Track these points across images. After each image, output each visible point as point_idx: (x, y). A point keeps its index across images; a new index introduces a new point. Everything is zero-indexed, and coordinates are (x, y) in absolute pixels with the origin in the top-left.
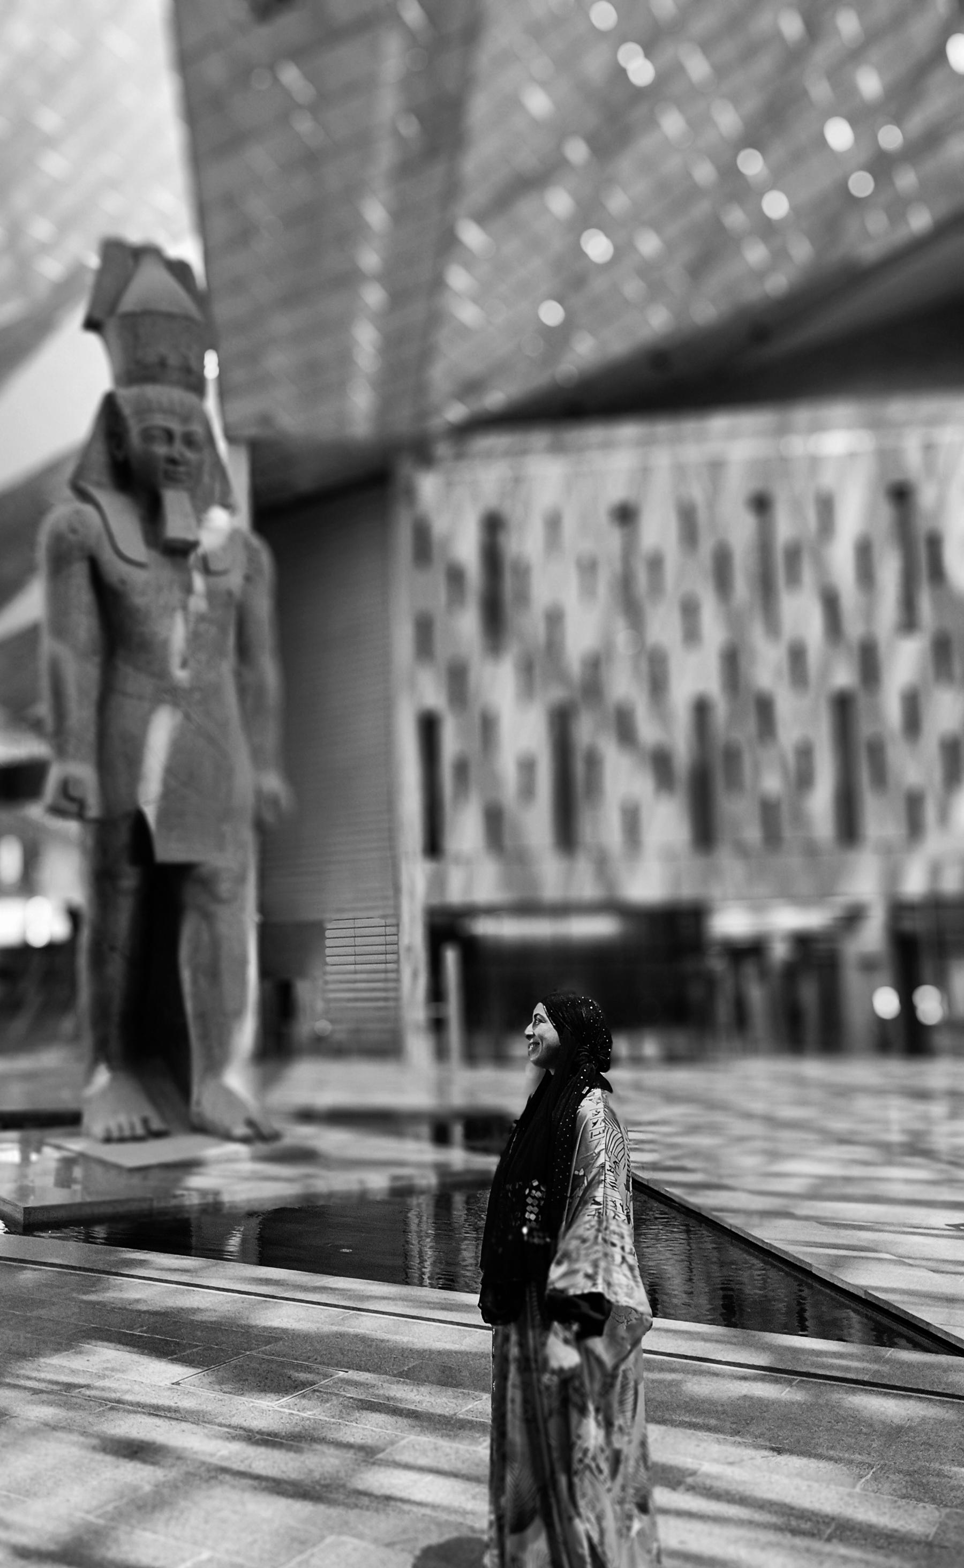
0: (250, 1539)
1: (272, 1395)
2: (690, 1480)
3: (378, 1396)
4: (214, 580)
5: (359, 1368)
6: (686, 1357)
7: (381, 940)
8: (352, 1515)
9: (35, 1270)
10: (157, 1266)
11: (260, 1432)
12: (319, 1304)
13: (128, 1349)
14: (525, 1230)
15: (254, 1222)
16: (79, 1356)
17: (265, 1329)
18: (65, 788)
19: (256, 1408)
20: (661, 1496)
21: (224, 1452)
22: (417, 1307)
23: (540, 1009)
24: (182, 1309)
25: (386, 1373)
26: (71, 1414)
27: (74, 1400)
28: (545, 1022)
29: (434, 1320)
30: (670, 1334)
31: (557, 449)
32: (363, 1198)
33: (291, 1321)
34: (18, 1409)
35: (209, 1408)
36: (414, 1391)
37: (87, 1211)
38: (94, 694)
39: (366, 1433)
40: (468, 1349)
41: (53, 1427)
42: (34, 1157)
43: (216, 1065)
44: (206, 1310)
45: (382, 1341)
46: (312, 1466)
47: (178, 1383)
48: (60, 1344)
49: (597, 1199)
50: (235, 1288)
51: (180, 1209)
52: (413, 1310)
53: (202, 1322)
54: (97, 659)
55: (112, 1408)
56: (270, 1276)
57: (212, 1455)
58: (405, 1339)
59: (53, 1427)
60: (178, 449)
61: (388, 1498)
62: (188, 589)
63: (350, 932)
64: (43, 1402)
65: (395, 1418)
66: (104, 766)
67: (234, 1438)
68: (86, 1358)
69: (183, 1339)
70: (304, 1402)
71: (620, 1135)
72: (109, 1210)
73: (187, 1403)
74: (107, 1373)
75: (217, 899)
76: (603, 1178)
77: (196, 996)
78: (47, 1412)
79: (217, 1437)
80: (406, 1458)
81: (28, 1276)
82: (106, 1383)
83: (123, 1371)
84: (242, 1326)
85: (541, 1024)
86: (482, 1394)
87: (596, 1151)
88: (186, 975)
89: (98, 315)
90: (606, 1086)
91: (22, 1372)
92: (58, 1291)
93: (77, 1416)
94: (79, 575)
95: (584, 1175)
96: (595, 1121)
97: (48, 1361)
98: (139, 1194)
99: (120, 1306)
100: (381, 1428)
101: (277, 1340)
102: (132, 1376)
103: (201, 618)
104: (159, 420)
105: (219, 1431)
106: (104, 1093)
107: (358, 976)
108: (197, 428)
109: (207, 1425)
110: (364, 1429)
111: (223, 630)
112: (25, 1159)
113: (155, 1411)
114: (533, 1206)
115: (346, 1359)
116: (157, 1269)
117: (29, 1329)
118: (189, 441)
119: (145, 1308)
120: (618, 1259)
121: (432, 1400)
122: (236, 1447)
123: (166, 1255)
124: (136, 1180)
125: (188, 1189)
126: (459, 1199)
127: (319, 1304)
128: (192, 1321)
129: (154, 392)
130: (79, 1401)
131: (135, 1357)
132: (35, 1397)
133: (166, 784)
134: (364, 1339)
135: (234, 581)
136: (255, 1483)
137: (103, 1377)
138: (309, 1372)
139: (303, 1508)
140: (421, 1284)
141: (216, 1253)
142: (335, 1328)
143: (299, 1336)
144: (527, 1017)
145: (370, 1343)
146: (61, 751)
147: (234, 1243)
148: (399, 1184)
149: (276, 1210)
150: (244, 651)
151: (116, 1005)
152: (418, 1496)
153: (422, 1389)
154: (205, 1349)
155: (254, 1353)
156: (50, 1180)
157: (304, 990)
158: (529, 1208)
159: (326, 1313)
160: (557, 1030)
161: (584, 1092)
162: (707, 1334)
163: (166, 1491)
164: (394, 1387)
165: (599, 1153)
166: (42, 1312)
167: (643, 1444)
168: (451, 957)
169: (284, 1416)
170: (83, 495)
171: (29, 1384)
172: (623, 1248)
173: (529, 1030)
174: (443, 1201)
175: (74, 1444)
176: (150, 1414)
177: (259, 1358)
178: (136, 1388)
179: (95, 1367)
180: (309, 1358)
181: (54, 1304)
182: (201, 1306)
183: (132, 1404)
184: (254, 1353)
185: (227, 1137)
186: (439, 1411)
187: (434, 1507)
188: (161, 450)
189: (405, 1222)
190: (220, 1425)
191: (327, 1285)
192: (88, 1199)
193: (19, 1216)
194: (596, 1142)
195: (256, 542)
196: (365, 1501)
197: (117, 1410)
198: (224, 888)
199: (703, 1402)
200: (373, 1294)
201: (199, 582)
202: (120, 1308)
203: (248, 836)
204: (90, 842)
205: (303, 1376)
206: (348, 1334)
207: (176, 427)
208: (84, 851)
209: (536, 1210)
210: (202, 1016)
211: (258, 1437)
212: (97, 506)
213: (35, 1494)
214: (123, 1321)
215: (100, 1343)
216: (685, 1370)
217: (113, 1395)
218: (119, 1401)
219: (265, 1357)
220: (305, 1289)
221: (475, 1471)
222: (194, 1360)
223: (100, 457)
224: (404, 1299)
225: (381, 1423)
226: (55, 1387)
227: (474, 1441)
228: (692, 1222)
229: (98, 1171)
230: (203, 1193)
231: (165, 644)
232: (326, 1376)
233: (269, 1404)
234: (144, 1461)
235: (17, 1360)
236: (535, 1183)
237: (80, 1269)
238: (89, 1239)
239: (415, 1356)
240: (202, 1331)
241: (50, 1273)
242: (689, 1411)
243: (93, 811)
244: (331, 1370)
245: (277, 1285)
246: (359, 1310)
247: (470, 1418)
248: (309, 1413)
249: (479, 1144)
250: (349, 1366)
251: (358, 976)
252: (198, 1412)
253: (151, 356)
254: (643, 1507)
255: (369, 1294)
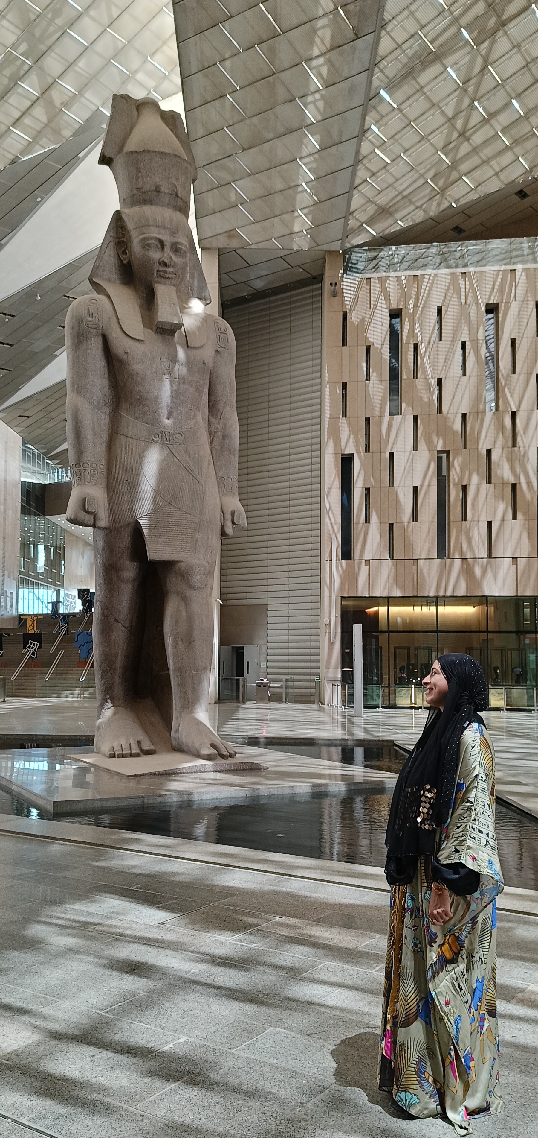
0: (214, 1029)
1: (229, 933)
2: (520, 995)
3: (303, 935)
4: (191, 352)
5: (290, 916)
6: (519, 912)
7: (308, 618)
8: (285, 1014)
9: (62, 845)
10: (148, 843)
11: (220, 957)
12: (262, 871)
13: (128, 899)
14: (419, 820)
15: (215, 814)
16: (94, 904)
17: (224, 887)
18: (83, 504)
19: (218, 941)
20: (501, 1006)
21: (196, 970)
22: (331, 875)
23: (436, 665)
24: (165, 873)
25: (308, 919)
26: (88, 943)
27: (90, 934)
28: (439, 674)
29: (342, 884)
30: (508, 896)
31: (444, 260)
32: (292, 799)
33: (242, 882)
34: (52, 939)
35: (185, 941)
36: (329, 931)
37: (98, 804)
38: (105, 436)
39: (294, 959)
40: (366, 904)
41: (72, 951)
42: (58, 767)
43: (190, 705)
44: (183, 874)
45: (306, 897)
46: (257, 981)
47: (163, 923)
48: (80, 895)
49: (469, 799)
50: (202, 859)
51: (163, 804)
52: (327, 876)
53: (179, 882)
54: (107, 410)
55: (117, 940)
56: (227, 851)
57: (187, 972)
58: (322, 896)
59: (72, 951)
60: (168, 255)
61: (310, 1003)
62: (174, 359)
63: (286, 613)
64: (69, 935)
65: (315, 949)
66: (111, 488)
67: (202, 961)
68: (99, 905)
69: (167, 893)
70: (252, 938)
71: (490, 756)
72: (114, 804)
73: (169, 937)
74: (113, 915)
75: (191, 587)
76: (476, 785)
77: (175, 655)
78: (71, 941)
79: (190, 960)
80: (322, 976)
81: (56, 848)
82: (113, 922)
83: (125, 914)
84: (208, 886)
85: (436, 675)
86: (376, 934)
87: (473, 766)
88: (169, 641)
89: (108, 154)
90: (481, 721)
91: (54, 914)
92: (78, 859)
93: (95, 945)
94: (95, 346)
95: (464, 783)
96: (473, 745)
97: (72, 907)
98: (134, 793)
99: (122, 870)
100: (305, 956)
101: (232, 895)
102: (131, 918)
103: (182, 380)
104: (155, 233)
105: (193, 956)
106: (109, 722)
107: (291, 644)
108: (182, 240)
109: (183, 952)
110: (293, 957)
111: (198, 390)
112: (52, 768)
113: (148, 942)
114: (426, 803)
115: (280, 909)
116: (148, 846)
117: (58, 885)
118: (176, 249)
119: (140, 872)
120: (484, 842)
121: (341, 937)
122: (203, 967)
123: (154, 836)
124: (132, 783)
125: (169, 791)
126: (359, 803)
127: (262, 871)
128: (173, 881)
129: (148, 210)
130: (94, 934)
131: (133, 905)
132: (63, 931)
133: (155, 502)
134: (293, 896)
135: (207, 354)
136: (218, 992)
137: (111, 918)
138: (255, 918)
139: (249, 1008)
140: (332, 859)
141: (187, 835)
142: (273, 888)
143: (247, 893)
144: (427, 669)
145: (297, 898)
146: (80, 477)
147: (200, 830)
148: (317, 790)
149: (230, 807)
150: (213, 405)
151: (119, 662)
152: (331, 1002)
153: (334, 930)
154: (182, 901)
155: (216, 903)
156: (69, 783)
157: (250, 654)
158: (423, 804)
159: (266, 877)
160: (447, 680)
161: (465, 725)
162: (534, 896)
163: (155, 996)
164: (314, 928)
165: (475, 767)
166: (67, 874)
167: (494, 970)
168: (358, 629)
169: (237, 946)
170: (97, 287)
171: (59, 922)
172: (487, 835)
173: (427, 679)
174: (347, 803)
175: (91, 963)
176: (144, 944)
177: (219, 907)
178: (134, 926)
179: (105, 911)
180: (255, 908)
181: (75, 868)
182: (179, 871)
183: (130, 936)
184: (216, 903)
185: (198, 756)
186: (345, 945)
187: (342, 1010)
188: (156, 255)
189: (321, 816)
190: (193, 952)
191: (267, 858)
192: (98, 797)
193: (50, 808)
194: (473, 760)
195: (224, 324)
196: (294, 1005)
197: (121, 941)
198: (197, 579)
199: (531, 943)
200: (300, 865)
201: (181, 354)
202: (122, 872)
203: (215, 541)
204: (101, 544)
205: (251, 920)
206: (283, 892)
207: (167, 238)
208: (95, 549)
209: (428, 805)
210: (180, 670)
211: (219, 960)
212: (108, 296)
213: (64, 997)
214: (124, 880)
215: (108, 895)
216: (519, 922)
217: (118, 931)
218: (122, 935)
219: (224, 907)
220: (253, 861)
221: (376, 986)
222: (174, 908)
223: (110, 259)
224: (321, 869)
225: (305, 953)
226: (77, 925)
227: (370, 966)
228: (525, 820)
229: (106, 777)
230: (180, 793)
231: (157, 399)
232: (267, 920)
233: (227, 938)
234: (140, 976)
235: (50, 906)
236: (428, 787)
237: (94, 844)
238: (98, 824)
239: (329, 908)
240: (179, 889)
241: (73, 847)
242: (520, 949)
243: (103, 522)
244: (270, 917)
245: (232, 858)
246: (290, 875)
247: (367, 950)
248: (255, 945)
249: (373, 763)
250: (282, 914)
251: (291, 644)
252: (177, 942)
253: (148, 184)
254: (492, 1013)
255: (297, 865)
